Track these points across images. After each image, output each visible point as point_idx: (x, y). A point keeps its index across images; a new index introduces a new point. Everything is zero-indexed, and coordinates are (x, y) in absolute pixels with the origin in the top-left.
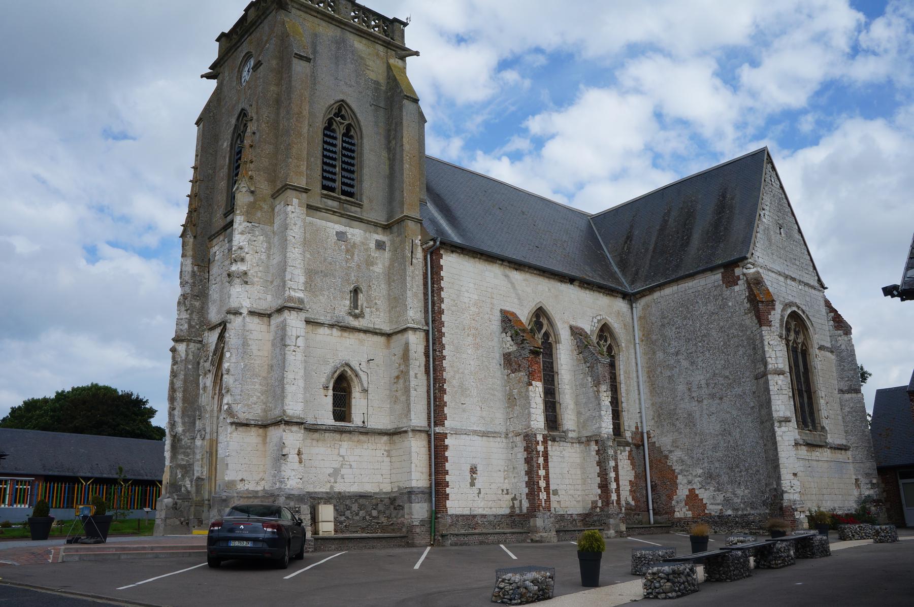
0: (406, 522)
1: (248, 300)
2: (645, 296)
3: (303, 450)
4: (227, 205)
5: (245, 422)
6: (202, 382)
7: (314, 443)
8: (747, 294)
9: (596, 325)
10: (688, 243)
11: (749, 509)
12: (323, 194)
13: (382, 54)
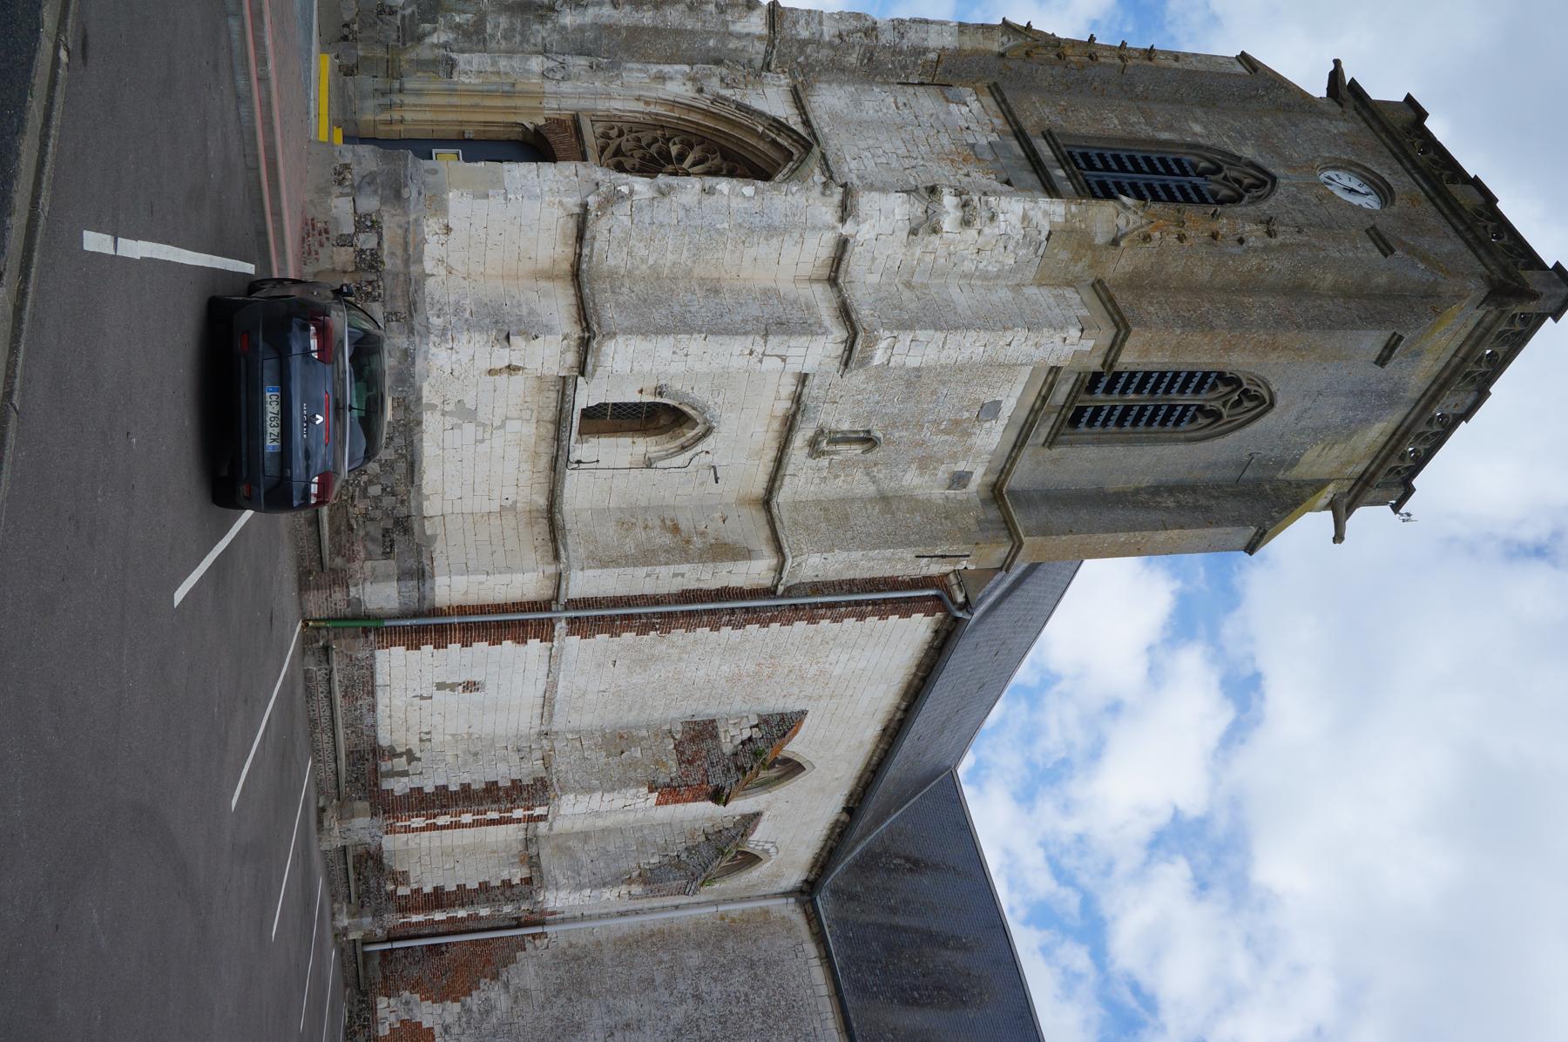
0: (356, 565)
1: (872, 235)
2: (809, 922)
3: (518, 378)
5: (588, 235)
6: (676, 72)
10: (907, 1002)
13: (1350, 470)
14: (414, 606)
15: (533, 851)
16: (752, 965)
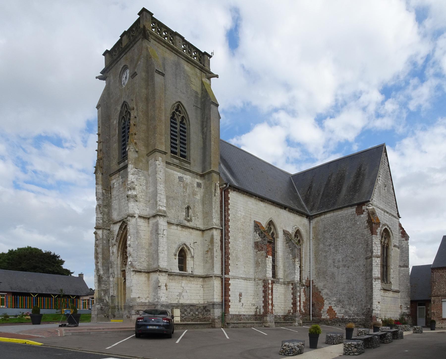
0: (211, 317)
1: (138, 210)
2: (317, 217)
3: (168, 284)
4: (119, 157)
5: (139, 270)
7: (171, 281)
8: (367, 219)
9: (294, 230)
11: (356, 316)
12: (172, 156)
13: (199, 74)
14: (221, 306)
15: (286, 283)
16: (324, 232)
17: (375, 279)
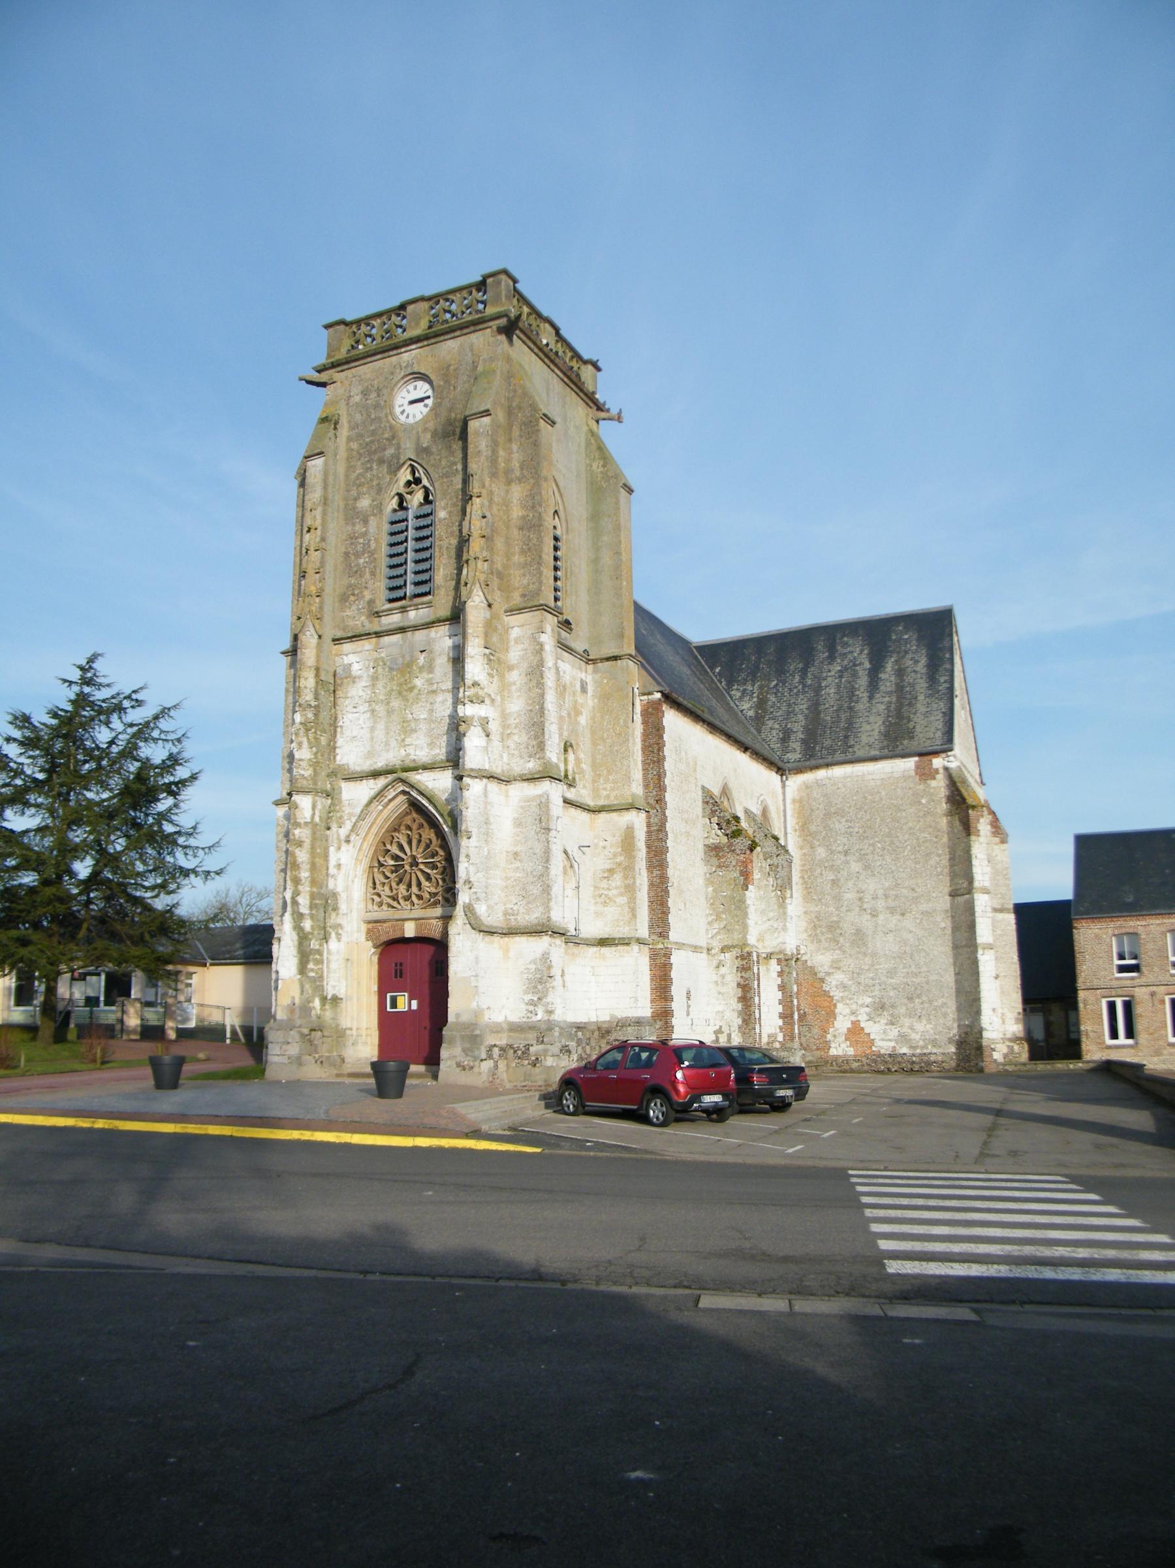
17: (984, 949)
